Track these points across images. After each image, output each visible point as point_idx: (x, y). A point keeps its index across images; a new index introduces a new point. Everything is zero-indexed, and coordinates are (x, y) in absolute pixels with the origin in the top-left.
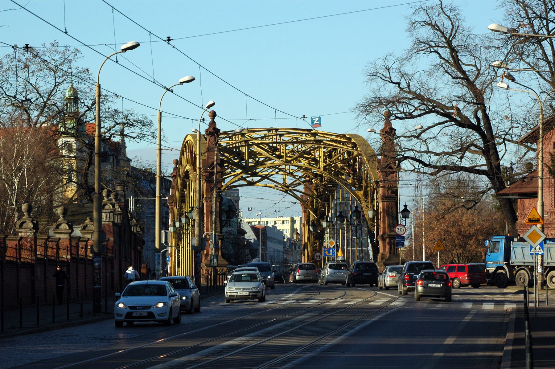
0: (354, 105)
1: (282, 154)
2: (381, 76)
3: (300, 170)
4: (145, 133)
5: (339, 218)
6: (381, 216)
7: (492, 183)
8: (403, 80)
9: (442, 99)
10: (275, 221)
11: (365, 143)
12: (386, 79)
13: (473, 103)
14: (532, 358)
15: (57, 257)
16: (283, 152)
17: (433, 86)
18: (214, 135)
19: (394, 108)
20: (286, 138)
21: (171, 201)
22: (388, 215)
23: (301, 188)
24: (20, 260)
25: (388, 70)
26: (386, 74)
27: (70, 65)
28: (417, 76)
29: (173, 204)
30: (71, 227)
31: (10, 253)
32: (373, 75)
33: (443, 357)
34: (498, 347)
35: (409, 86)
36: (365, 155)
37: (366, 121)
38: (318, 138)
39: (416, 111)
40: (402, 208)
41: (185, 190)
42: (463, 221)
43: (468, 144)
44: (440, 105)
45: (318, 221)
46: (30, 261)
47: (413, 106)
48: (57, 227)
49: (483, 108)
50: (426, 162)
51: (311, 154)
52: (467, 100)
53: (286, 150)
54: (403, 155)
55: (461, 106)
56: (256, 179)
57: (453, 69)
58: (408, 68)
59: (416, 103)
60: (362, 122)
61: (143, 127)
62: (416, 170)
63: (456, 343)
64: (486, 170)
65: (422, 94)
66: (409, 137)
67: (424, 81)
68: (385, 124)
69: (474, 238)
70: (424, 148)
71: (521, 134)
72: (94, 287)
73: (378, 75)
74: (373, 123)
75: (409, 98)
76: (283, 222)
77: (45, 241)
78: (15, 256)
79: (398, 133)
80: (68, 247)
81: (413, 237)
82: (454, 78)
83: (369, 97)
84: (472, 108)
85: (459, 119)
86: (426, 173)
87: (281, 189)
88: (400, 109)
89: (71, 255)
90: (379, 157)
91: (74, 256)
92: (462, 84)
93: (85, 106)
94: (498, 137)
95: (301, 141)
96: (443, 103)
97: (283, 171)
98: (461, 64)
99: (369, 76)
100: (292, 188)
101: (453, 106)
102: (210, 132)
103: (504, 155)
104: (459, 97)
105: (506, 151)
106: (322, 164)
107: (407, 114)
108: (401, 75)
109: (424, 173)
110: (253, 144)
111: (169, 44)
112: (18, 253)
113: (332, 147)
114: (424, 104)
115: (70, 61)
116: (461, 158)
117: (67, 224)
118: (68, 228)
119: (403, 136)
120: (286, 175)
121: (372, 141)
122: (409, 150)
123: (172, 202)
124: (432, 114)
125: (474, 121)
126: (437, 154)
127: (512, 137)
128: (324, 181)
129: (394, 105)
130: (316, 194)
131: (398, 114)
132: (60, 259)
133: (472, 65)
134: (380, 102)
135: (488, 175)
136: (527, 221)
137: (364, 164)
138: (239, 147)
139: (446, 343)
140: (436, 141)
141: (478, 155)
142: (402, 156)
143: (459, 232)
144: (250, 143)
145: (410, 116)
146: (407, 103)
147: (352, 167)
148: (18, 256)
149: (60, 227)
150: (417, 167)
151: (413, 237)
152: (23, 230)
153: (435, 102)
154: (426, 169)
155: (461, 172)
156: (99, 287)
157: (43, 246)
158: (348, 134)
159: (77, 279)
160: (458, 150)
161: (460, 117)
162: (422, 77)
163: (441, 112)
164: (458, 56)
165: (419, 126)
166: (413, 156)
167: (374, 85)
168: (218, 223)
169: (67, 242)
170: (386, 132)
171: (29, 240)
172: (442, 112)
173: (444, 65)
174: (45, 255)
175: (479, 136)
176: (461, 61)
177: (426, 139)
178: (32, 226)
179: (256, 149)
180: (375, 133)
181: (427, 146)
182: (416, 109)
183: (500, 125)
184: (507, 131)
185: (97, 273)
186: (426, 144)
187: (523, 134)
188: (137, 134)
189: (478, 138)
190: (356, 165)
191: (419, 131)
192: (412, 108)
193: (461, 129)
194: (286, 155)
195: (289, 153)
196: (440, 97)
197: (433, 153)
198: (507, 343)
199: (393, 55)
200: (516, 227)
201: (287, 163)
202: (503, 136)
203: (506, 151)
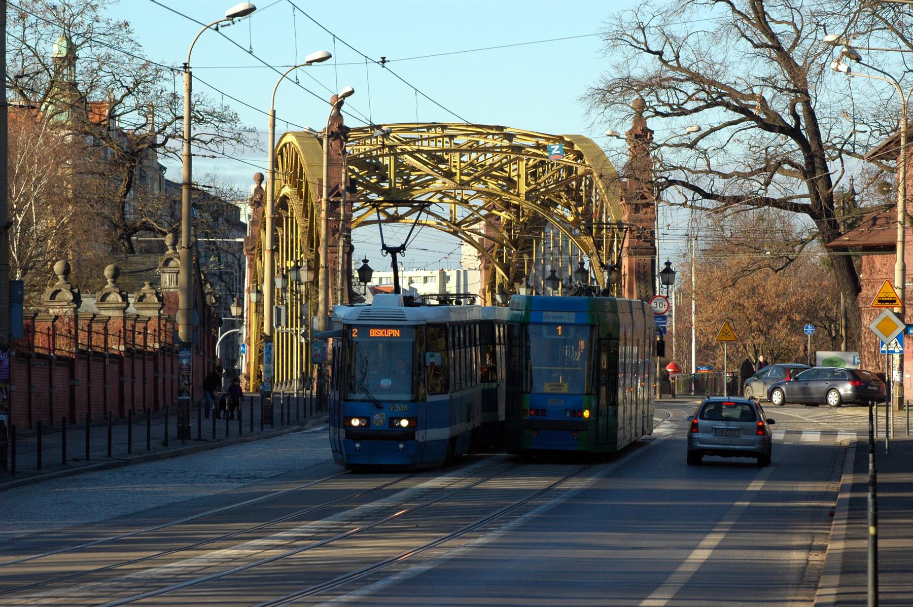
0: (583, 91)
1: (454, 170)
2: (630, 39)
3: (480, 196)
4: (226, 134)
5: (550, 282)
6: (626, 281)
7: (819, 225)
8: (667, 46)
9: (735, 82)
10: (410, 278)
11: (599, 155)
12: (638, 45)
13: (789, 90)
14: (876, 510)
15: (105, 348)
16: (455, 166)
17: (719, 59)
18: (340, 138)
19: (652, 98)
20: (461, 140)
21: (250, 248)
22: (638, 279)
23: (480, 226)
24: (54, 353)
25: (643, 29)
26: (639, 36)
27: (97, 16)
28: (691, 40)
29: (255, 252)
30: (125, 298)
31: (40, 341)
32: (616, 39)
33: (749, 507)
34: (831, 496)
35: (677, 57)
36: (601, 176)
37: (605, 119)
38: (516, 142)
39: (690, 102)
40: (663, 267)
41: (279, 229)
42: (768, 287)
43: (779, 159)
44: (732, 92)
45: (511, 285)
46: (67, 354)
47: (686, 93)
48: (103, 299)
49: (806, 98)
50: (705, 190)
51: (502, 170)
52: (779, 85)
53: (461, 162)
54: (666, 178)
55: (768, 94)
56: (402, 210)
57: (754, 29)
58: (676, 29)
59: (690, 88)
60: (598, 120)
61: (221, 125)
62: (689, 203)
63: (764, 489)
64: (808, 205)
65: (701, 72)
66: (676, 146)
67: (704, 49)
68: (635, 122)
69: (785, 317)
70: (701, 164)
71: (870, 143)
72: (180, 398)
73: (625, 37)
74: (615, 122)
75: (677, 80)
76: (426, 279)
77: (88, 322)
78: (47, 346)
79: (657, 138)
80: (120, 332)
81: (674, 314)
82: (756, 46)
83: (609, 78)
84: (787, 98)
85: (763, 116)
86: (707, 209)
87: (447, 229)
88: (662, 98)
89: (125, 344)
90: (625, 180)
91: (128, 346)
92: (770, 58)
93: (123, 86)
94: (829, 148)
95: (485, 147)
96: (738, 89)
97: (451, 197)
98: (768, 20)
99: (609, 41)
100: (466, 227)
101: (753, 94)
102: (332, 132)
103: (840, 178)
104: (764, 80)
105: (843, 172)
106: (523, 189)
107: (675, 107)
108: (665, 38)
109: (702, 209)
110: (404, 152)
111: (383, 67)
112: (51, 342)
113: (539, 159)
114: (704, 90)
115: (94, 8)
116: (767, 184)
117: (120, 293)
118: (120, 300)
119: (667, 145)
120: (455, 204)
121: (613, 153)
122: (675, 168)
123: (253, 249)
124: (717, 108)
125: (789, 121)
126: (725, 176)
127: (854, 147)
128: (523, 216)
129: (652, 90)
130: (507, 237)
131: (660, 106)
132: (111, 352)
133: (787, 22)
134: (628, 85)
135: (813, 216)
136: (876, 302)
137: (596, 189)
138: (377, 157)
139: (749, 489)
140: (723, 153)
141: (795, 179)
142: (664, 180)
143: (760, 308)
144: (399, 151)
145: (681, 112)
146: (675, 89)
147: (575, 196)
148: (51, 346)
149: (108, 299)
150: (690, 197)
151: (674, 314)
152: (55, 304)
153: (723, 86)
154: (707, 203)
155: (766, 207)
156: (188, 398)
157: (85, 331)
158: (568, 136)
159: (133, 383)
160: (761, 169)
161: (765, 114)
162: (701, 43)
163: (734, 106)
164: (763, 7)
165: (695, 128)
166: (683, 179)
167: (618, 57)
168: (346, 291)
169: (119, 324)
170: (637, 136)
171: (66, 320)
172: (735, 103)
173: (739, 23)
174: (88, 345)
175: (797, 145)
176: (768, 15)
177: (706, 150)
178: (71, 298)
179: (409, 160)
180: (618, 137)
181: (708, 161)
182: (690, 98)
183: (834, 127)
184: (846, 137)
185: (183, 376)
186: (706, 157)
187: (872, 141)
188: (213, 137)
189: (795, 149)
190: (582, 191)
191: (694, 136)
192: (682, 97)
193: (767, 134)
194: (461, 170)
195: (465, 168)
196: (732, 80)
197: (718, 173)
198: (843, 489)
199: (651, 4)
200: (858, 304)
201: (463, 185)
202: (839, 146)
203: (843, 172)
